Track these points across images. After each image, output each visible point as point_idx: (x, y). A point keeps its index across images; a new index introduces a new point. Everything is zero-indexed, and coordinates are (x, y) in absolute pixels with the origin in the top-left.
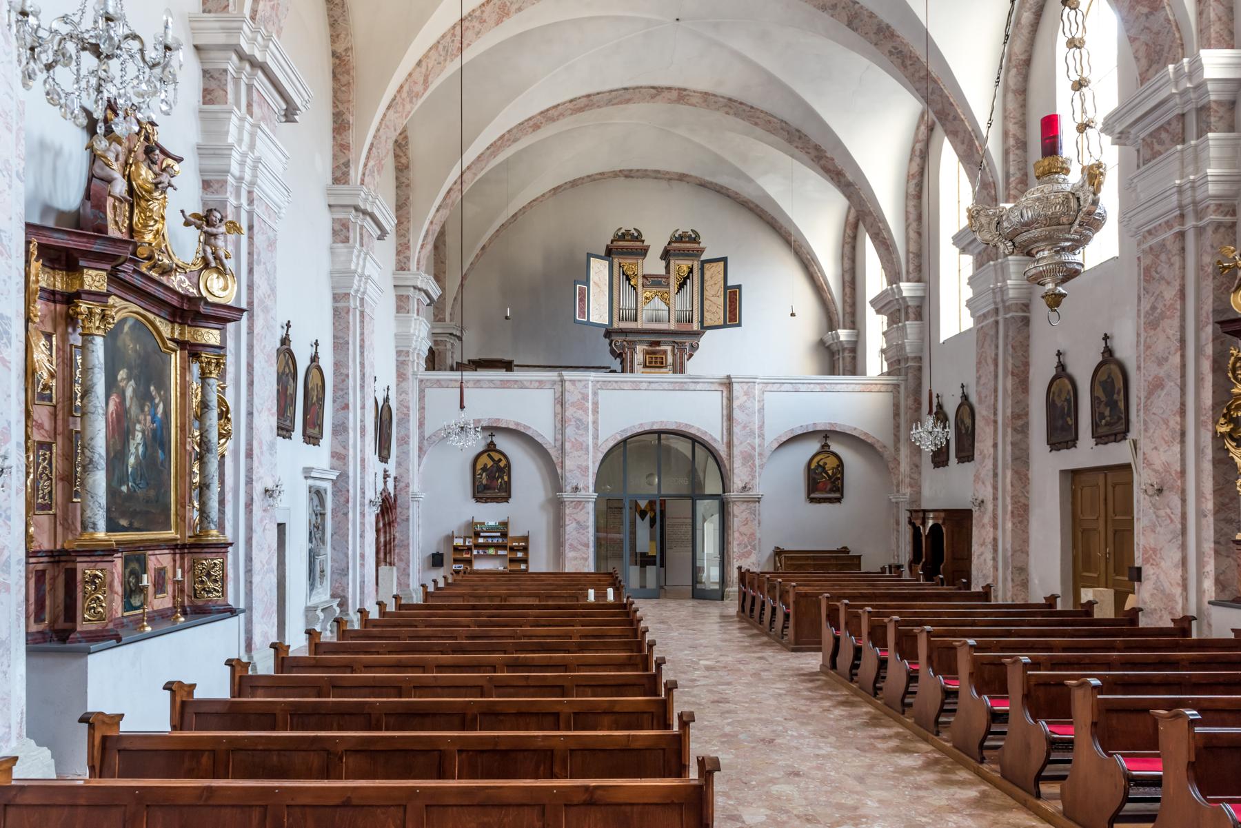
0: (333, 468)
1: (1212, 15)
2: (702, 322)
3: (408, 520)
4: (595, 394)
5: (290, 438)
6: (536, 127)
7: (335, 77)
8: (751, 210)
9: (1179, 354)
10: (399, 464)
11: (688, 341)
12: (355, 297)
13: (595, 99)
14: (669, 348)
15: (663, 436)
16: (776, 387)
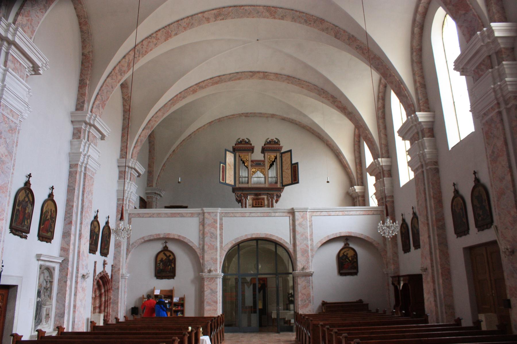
0: (61, 256)
1: (494, 10)
2: (282, 183)
3: (118, 288)
4: (221, 219)
5: (26, 237)
6: (194, 91)
7: (82, 64)
8: (308, 130)
9: (509, 174)
10: (115, 258)
11: (275, 193)
12: (81, 166)
13: (223, 78)
14: (265, 197)
15: (259, 242)
16: (318, 213)
